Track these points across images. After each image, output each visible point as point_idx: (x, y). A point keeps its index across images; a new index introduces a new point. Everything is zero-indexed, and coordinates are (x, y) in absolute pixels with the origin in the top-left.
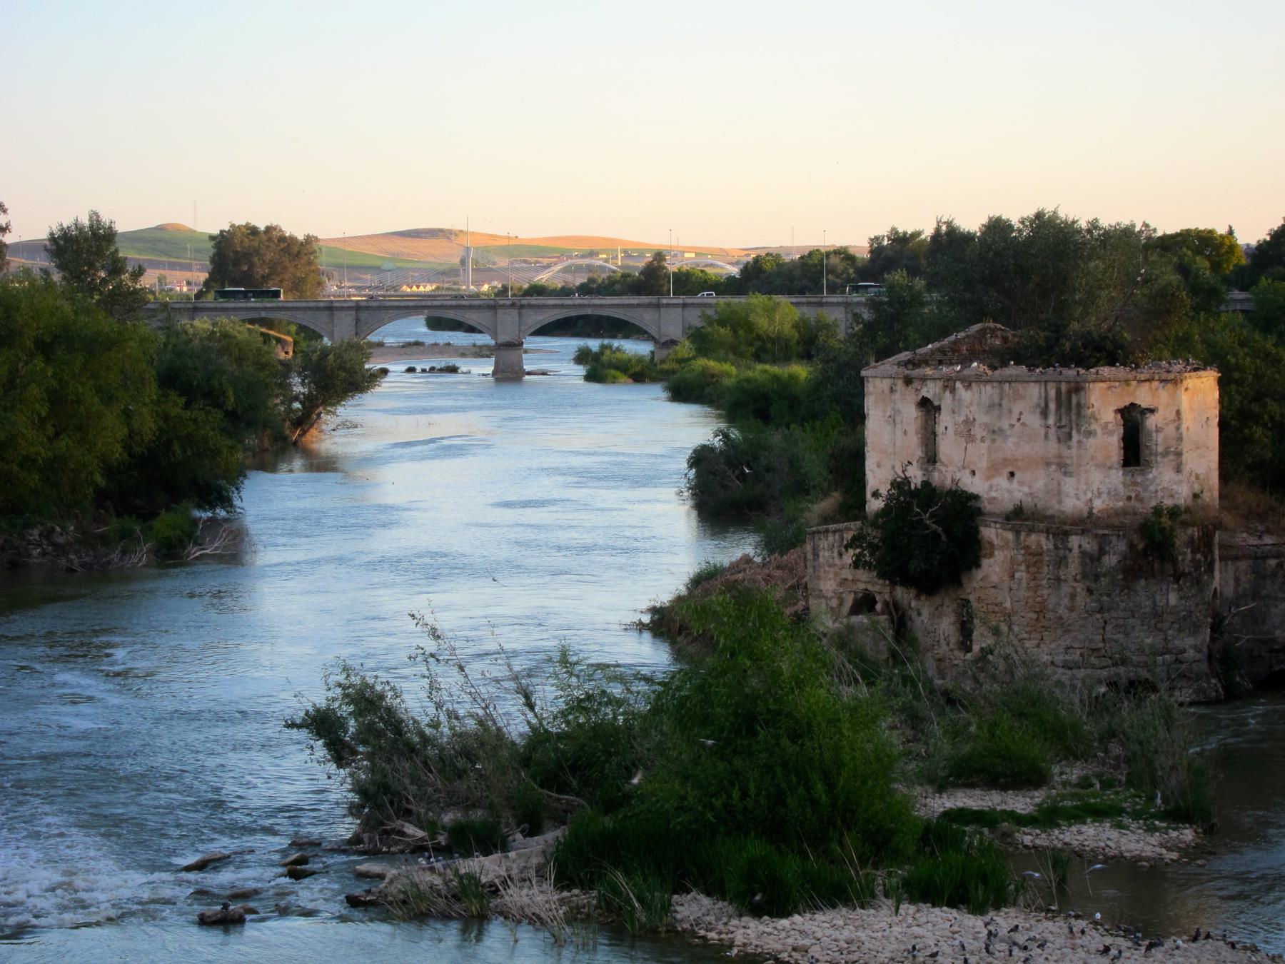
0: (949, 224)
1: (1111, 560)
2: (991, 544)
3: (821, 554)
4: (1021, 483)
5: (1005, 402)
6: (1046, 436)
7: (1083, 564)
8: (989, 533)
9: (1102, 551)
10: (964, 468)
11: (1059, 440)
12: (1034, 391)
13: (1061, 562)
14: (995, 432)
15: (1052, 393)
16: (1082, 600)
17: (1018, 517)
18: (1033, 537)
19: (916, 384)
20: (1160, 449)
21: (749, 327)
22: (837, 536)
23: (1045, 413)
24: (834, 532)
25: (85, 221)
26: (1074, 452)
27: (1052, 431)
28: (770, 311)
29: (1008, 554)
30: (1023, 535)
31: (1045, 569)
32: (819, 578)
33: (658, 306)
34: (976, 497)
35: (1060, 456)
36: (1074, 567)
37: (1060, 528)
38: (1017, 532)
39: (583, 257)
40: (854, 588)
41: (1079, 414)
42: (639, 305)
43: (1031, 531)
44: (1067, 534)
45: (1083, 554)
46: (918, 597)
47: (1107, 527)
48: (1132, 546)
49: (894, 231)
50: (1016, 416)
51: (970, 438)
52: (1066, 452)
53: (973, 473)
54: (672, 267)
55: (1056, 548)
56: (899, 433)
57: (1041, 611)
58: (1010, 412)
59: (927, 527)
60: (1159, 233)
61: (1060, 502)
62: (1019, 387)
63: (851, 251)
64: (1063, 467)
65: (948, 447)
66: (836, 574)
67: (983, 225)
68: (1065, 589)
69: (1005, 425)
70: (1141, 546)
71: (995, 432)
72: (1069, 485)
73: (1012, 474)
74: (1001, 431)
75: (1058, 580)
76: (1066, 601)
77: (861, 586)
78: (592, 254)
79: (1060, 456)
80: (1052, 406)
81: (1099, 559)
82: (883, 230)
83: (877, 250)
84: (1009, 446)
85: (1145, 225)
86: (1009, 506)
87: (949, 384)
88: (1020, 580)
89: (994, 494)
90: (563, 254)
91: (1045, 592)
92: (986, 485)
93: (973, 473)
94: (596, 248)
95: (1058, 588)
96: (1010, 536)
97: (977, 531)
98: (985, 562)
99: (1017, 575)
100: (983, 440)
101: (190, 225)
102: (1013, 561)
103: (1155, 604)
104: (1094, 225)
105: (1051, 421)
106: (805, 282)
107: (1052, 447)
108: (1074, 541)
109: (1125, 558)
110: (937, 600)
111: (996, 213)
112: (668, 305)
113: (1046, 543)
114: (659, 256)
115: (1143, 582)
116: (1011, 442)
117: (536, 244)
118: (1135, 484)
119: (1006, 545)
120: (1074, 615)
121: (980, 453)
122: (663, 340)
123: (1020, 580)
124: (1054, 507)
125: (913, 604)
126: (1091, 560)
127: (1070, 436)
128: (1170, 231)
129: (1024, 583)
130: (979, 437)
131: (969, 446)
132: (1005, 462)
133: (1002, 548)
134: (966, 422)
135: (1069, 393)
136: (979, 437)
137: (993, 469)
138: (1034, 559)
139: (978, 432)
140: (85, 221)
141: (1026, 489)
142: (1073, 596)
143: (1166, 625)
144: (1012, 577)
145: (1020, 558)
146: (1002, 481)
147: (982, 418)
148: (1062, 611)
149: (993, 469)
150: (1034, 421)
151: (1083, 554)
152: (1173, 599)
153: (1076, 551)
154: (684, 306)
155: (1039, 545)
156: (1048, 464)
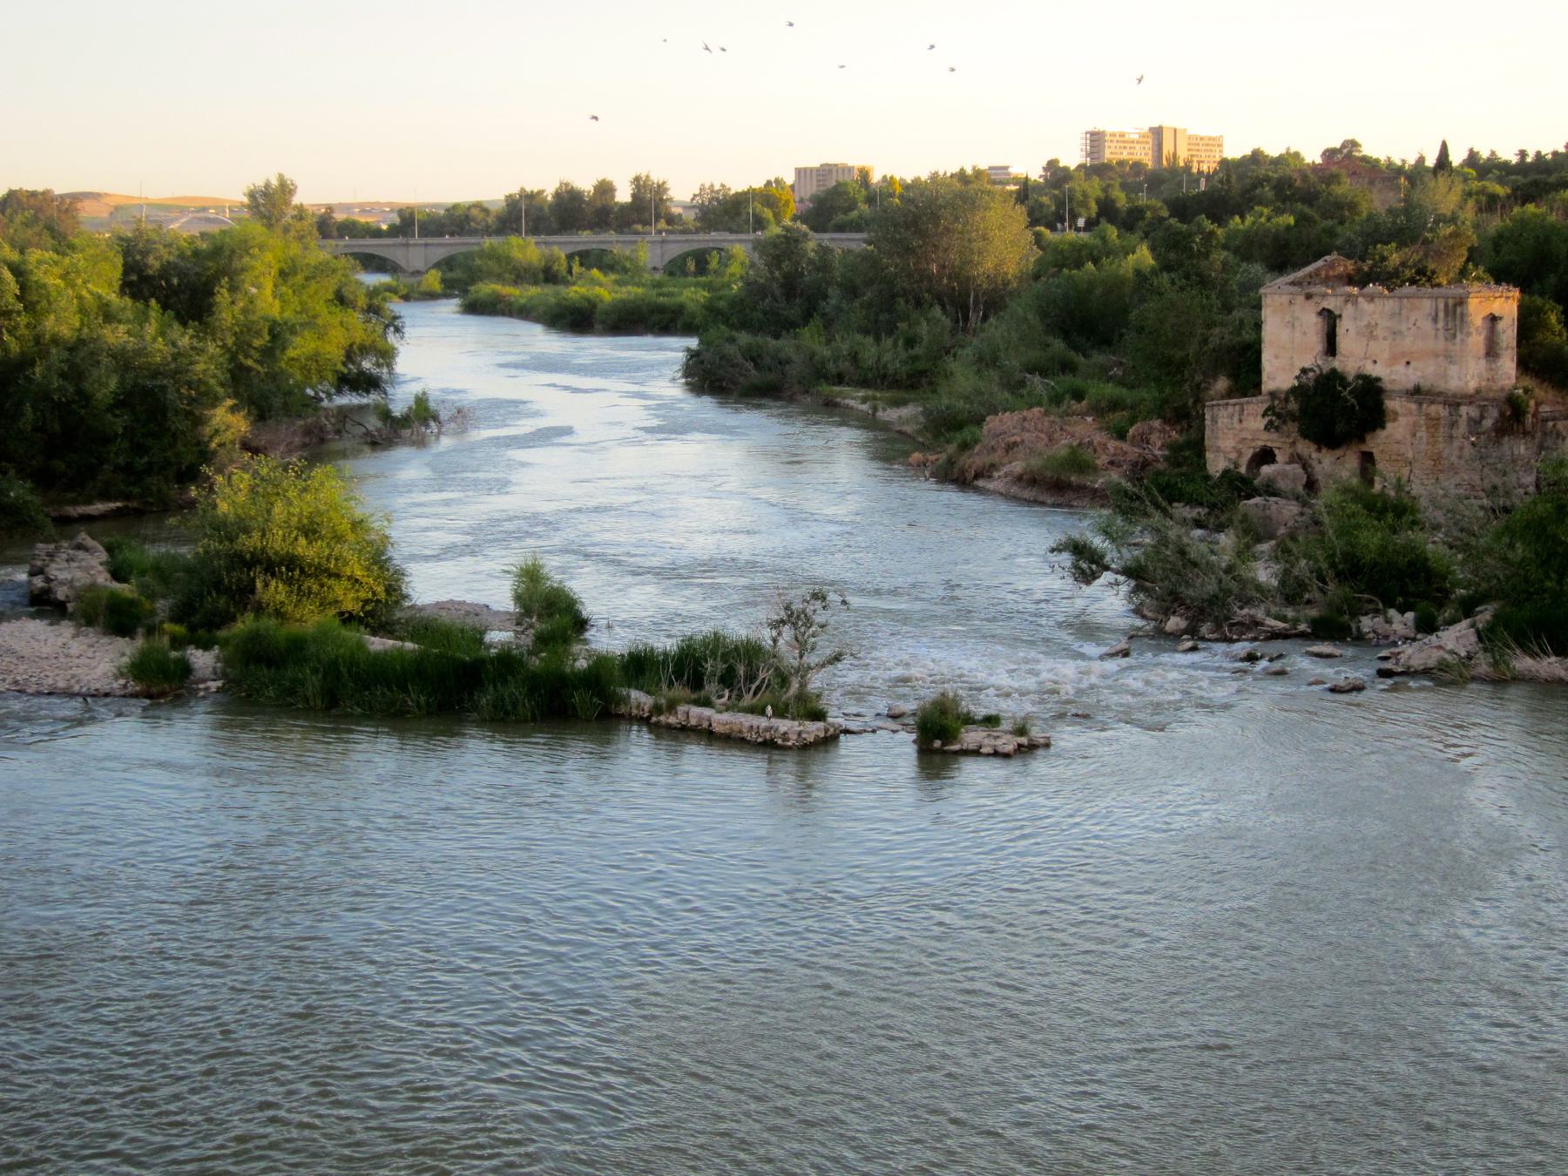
0: (567, 184)
1: (1488, 423)
2: (1396, 413)
3: (1220, 421)
4: (1416, 369)
5: (1404, 312)
6: (1436, 337)
7: (1468, 424)
8: (1391, 404)
9: (1482, 417)
10: (1365, 358)
11: (1446, 339)
12: (1427, 304)
13: (1453, 424)
14: (1396, 333)
15: (1441, 306)
16: (1468, 451)
17: (1417, 393)
18: (1433, 407)
19: (1316, 299)
20: (1504, 345)
21: (509, 260)
22: (1237, 408)
23: (1435, 320)
24: (1235, 405)
25: (275, 182)
26: (1458, 347)
27: (1441, 332)
28: (522, 248)
29: (1412, 419)
30: (1425, 406)
31: (1442, 430)
32: (1217, 438)
33: (407, 245)
34: (1378, 379)
35: (1446, 350)
36: (1463, 427)
37: (1454, 402)
38: (1420, 404)
39: (198, 212)
40: (1253, 444)
41: (1462, 320)
42: (394, 245)
43: (1432, 403)
44: (1459, 405)
45: (1470, 419)
46: (1319, 450)
47: (1486, 400)
48: (1502, 414)
49: (523, 190)
50: (1412, 322)
51: (1372, 336)
52: (1451, 347)
53: (1375, 362)
54: (339, 217)
55: (1451, 414)
56: (1298, 335)
57: (1437, 459)
58: (1408, 318)
59: (1347, 401)
60: (732, 192)
61: (1446, 382)
62: (1416, 301)
63: (485, 205)
64: (1449, 358)
65: (1344, 342)
66: (1235, 435)
67: (864, 174)
68: (1456, 444)
69: (1403, 328)
70: (1508, 413)
71: (1396, 333)
72: (1453, 370)
73: (1408, 363)
74: (1400, 332)
75: (1451, 437)
76: (1456, 453)
77: (1260, 443)
78: (204, 209)
79: (1446, 350)
80: (1441, 315)
81: (1480, 422)
82: (514, 190)
83: (512, 203)
84: (1407, 343)
85: (723, 185)
86: (1410, 386)
87: (1349, 298)
88: (1421, 438)
89: (1394, 377)
90: (182, 210)
91: (1441, 446)
92: (1388, 371)
93: (1375, 362)
94: (206, 205)
95: (1451, 442)
96: (1413, 406)
97: (1382, 404)
98: (1389, 426)
99: (1418, 434)
100: (1385, 339)
101: (136, 194)
102: (1415, 424)
103: (1513, 454)
104: (934, 176)
105: (1441, 325)
106: (453, 228)
107: (1441, 344)
108: (1464, 410)
109: (1497, 422)
110: (1339, 452)
111: (609, 178)
112: (415, 245)
113: (1442, 411)
114: (330, 209)
115: (1506, 439)
116: (1408, 341)
117: (170, 203)
118: (1491, 369)
119: (1410, 413)
120: (1462, 462)
121: (1381, 348)
122: (411, 270)
123: (1421, 438)
124: (1442, 386)
125: (1314, 455)
126: (1475, 423)
127: (1454, 336)
128: (740, 190)
129: (1425, 439)
130: (1381, 337)
131: (1371, 343)
132: (1403, 354)
133: (1405, 415)
134: (1368, 325)
135: (1455, 305)
136: (1381, 337)
137: (1394, 359)
138: (1433, 423)
139: (1379, 332)
140: (275, 182)
141: (1419, 374)
142: (1461, 448)
143: (1517, 468)
144: (1414, 435)
145: (1422, 422)
146: (1401, 368)
147: (1384, 323)
148: (1454, 459)
149: (1394, 359)
150: (1427, 325)
151: (1470, 419)
152: (1522, 448)
153: (1465, 416)
154: (426, 245)
155: (1438, 413)
156: (1437, 356)
